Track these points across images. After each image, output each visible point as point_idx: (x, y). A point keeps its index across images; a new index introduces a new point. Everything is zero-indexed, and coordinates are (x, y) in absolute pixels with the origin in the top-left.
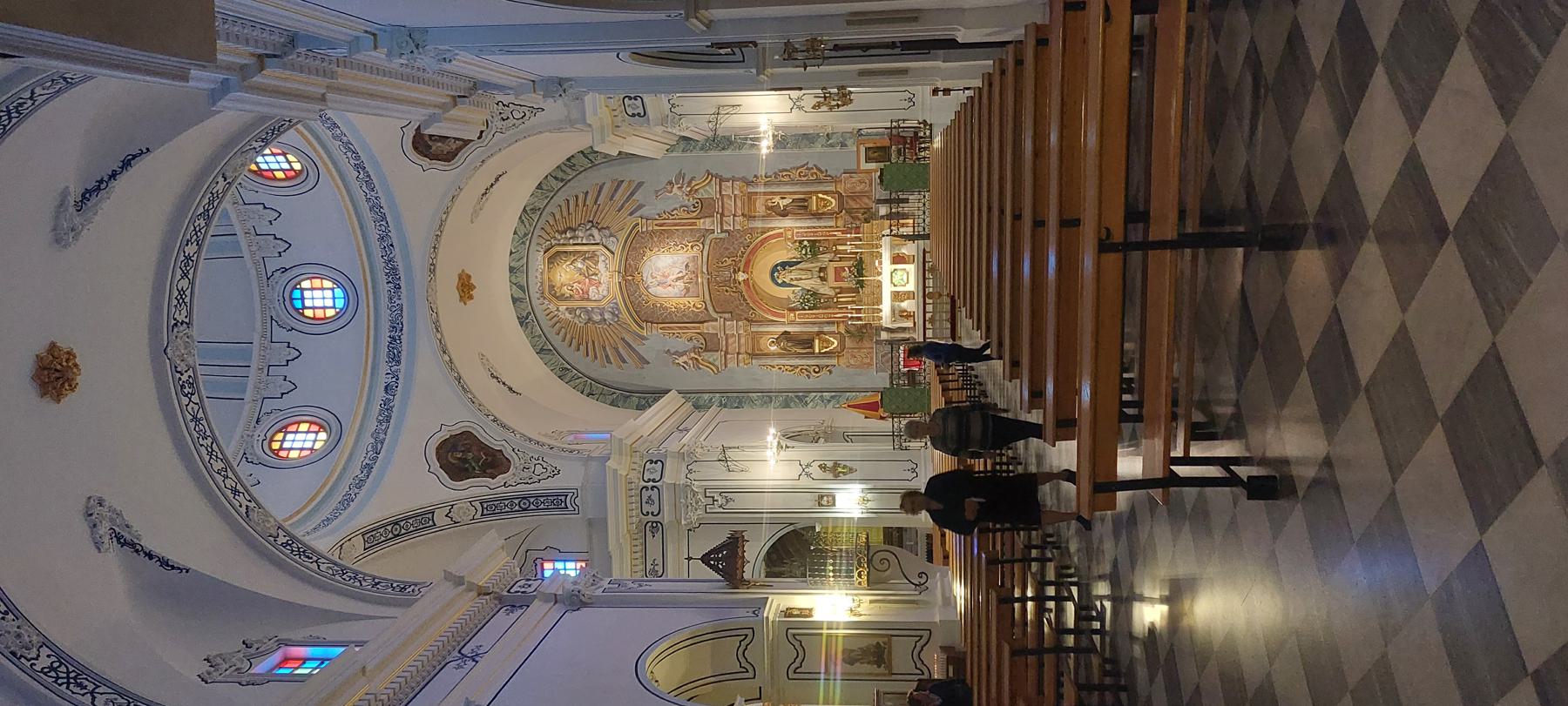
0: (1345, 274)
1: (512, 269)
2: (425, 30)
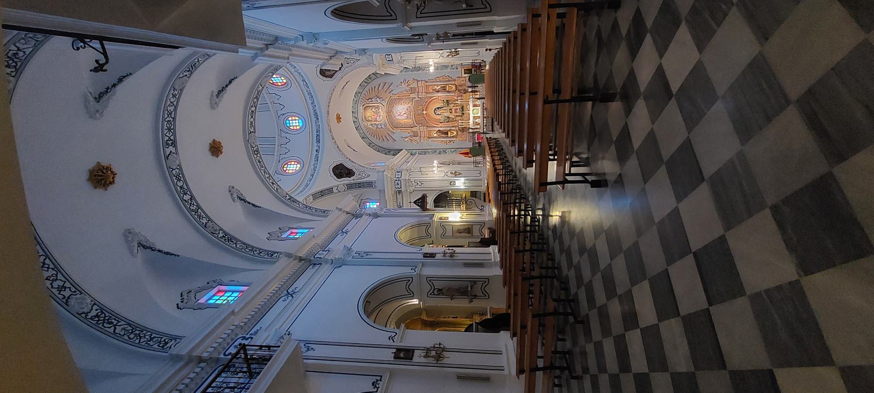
0: (630, 111)
2: (318, 34)
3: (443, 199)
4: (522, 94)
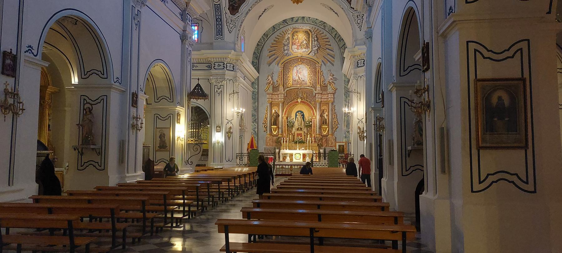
3: (201, 120)
4: (319, 206)
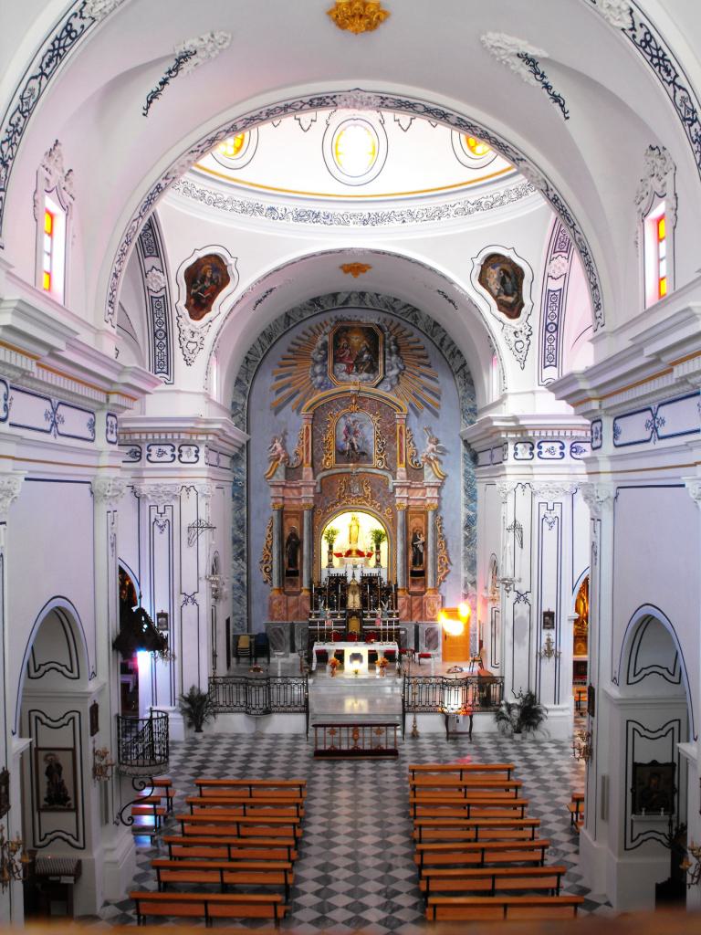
1: (363, 294)
